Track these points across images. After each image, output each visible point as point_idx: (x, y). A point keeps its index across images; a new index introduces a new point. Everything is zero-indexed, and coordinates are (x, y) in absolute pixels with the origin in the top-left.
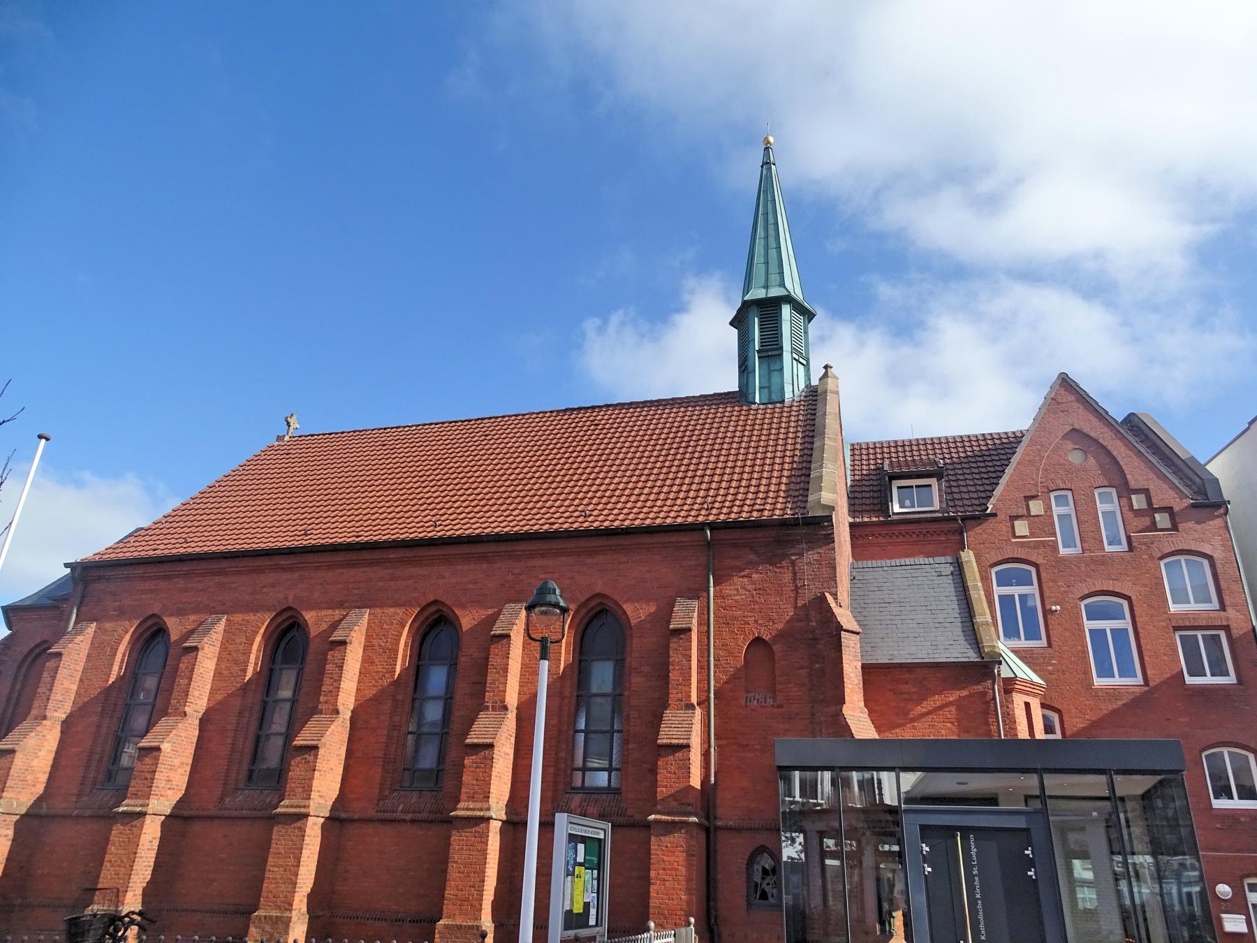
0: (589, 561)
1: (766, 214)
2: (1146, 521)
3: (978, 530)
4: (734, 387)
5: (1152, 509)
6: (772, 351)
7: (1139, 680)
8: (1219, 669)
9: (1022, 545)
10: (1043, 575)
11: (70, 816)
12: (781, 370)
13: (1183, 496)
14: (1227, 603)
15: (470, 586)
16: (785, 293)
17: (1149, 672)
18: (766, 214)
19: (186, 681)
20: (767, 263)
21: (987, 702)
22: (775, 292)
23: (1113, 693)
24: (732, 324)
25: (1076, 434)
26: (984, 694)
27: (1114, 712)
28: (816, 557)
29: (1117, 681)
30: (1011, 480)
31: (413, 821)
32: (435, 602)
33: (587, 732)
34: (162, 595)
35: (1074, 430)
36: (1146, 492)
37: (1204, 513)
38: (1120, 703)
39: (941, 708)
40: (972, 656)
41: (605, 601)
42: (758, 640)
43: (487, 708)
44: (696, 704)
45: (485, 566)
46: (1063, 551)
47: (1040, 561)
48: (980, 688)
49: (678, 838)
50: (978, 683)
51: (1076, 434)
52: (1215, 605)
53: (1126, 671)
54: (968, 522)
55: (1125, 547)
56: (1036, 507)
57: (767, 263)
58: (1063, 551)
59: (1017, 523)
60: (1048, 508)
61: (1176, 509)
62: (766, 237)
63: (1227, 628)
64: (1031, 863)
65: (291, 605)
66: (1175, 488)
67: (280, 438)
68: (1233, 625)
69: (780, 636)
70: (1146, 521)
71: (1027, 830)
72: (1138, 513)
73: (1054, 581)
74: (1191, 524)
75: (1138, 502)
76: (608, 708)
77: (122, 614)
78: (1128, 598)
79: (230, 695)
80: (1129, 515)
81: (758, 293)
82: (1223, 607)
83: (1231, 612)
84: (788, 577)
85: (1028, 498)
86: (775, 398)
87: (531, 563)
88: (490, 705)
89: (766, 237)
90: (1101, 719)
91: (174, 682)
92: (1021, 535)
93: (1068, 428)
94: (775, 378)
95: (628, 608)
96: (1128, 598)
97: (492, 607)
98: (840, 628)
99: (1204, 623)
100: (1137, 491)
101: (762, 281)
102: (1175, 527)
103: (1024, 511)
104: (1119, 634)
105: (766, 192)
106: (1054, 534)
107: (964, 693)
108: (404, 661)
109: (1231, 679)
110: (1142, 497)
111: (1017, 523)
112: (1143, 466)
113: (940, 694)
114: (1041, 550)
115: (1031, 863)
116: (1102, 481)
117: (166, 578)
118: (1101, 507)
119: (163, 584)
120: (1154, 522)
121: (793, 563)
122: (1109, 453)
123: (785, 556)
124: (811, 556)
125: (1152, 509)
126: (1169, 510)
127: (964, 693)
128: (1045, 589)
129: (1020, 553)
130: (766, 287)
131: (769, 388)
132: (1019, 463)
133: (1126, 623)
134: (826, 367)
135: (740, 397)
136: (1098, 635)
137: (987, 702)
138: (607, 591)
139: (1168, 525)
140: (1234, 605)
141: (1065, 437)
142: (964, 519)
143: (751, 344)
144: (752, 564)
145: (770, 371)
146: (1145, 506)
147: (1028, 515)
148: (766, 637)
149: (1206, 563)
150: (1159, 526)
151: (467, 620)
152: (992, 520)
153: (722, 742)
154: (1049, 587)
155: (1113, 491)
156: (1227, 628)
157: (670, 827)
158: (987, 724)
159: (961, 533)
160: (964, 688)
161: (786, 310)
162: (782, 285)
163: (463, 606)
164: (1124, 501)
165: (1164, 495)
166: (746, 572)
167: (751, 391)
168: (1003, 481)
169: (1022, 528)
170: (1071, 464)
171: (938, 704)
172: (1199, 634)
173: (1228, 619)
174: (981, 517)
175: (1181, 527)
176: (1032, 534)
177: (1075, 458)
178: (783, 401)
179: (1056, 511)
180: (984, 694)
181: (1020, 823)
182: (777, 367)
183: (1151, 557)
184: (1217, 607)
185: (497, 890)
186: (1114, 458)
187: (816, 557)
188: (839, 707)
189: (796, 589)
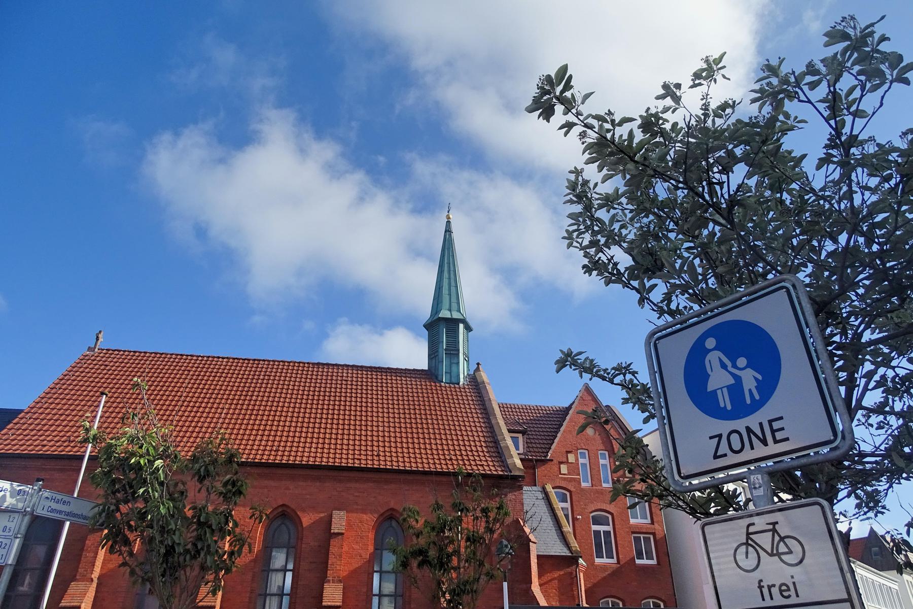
0: (386, 487)
1: (449, 263)
3: (543, 468)
4: (425, 366)
6: (453, 351)
7: (614, 561)
8: (650, 557)
9: (565, 479)
10: (574, 497)
12: (458, 363)
14: (655, 520)
15: (308, 496)
16: (462, 318)
17: (620, 556)
18: (449, 263)
19: (92, 555)
20: (450, 295)
21: (572, 578)
22: (456, 315)
23: (604, 567)
24: (425, 326)
26: (571, 573)
27: (604, 578)
28: (514, 497)
29: (605, 560)
30: (560, 441)
32: (283, 505)
34: (57, 484)
38: (607, 573)
39: (550, 581)
40: (565, 552)
41: (394, 513)
43: (329, 581)
45: (318, 484)
46: (584, 485)
47: (572, 489)
48: (569, 570)
50: (568, 567)
52: (649, 521)
53: (610, 556)
54: (538, 463)
56: (571, 458)
57: (450, 295)
58: (584, 485)
59: (562, 466)
60: (577, 460)
62: (449, 278)
63: (654, 534)
67: (89, 349)
68: (657, 532)
73: (579, 502)
78: (612, 514)
81: (445, 314)
82: (652, 523)
83: (656, 525)
85: (568, 452)
86: (454, 380)
87: (348, 485)
88: (331, 579)
89: (449, 278)
90: (599, 582)
91: (81, 555)
92: (844, 604)
94: (454, 368)
96: (612, 514)
97: (323, 512)
98: (530, 540)
99: (644, 531)
101: (447, 307)
103: (564, 460)
104: (607, 533)
105: (449, 249)
106: (579, 474)
107: (562, 573)
108: (259, 545)
109: (653, 562)
111: (562, 466)
113: (550, 573)
114: (573, 483)
116: (602, 447)
117: (62, 470)
118: (602, 462)
124: (511, 496)
127: (562, 573)
128: (574, 506)
129: (563, 484)
130: (450, 310)
131: (450, 373)
132: (564, 431)
135: (430, 375)
136: (597, 533)
137: (572, 578)
138: (396, 507)
140: (658, 522)
142: (537, 461)
143: (441, 345)
145: (451, 364)
147: (567, 462)
151: (307, 520)
152: (550, 463)
154: (576, 505)
155: (607, 453)
156: (654, 534)
158: (572, 590)
159: (534, 469)
160: (561, 570)
161: (461, 326)
162: (459, 311)
163: (304, 511)
167: (440, 373)
168: (556, 441)
169: (564, 469)
170: (588, 435)
171: (550, 578)
172: (642, 536)
173: (654, 529)
174: (544, 462)
176: (569, 474)
178: (458, 384)
179: (581, 461)
180: (571, 573)
182: (455, 361)
184: (650, 522)
187: (514, 497)
188: (529, 585)
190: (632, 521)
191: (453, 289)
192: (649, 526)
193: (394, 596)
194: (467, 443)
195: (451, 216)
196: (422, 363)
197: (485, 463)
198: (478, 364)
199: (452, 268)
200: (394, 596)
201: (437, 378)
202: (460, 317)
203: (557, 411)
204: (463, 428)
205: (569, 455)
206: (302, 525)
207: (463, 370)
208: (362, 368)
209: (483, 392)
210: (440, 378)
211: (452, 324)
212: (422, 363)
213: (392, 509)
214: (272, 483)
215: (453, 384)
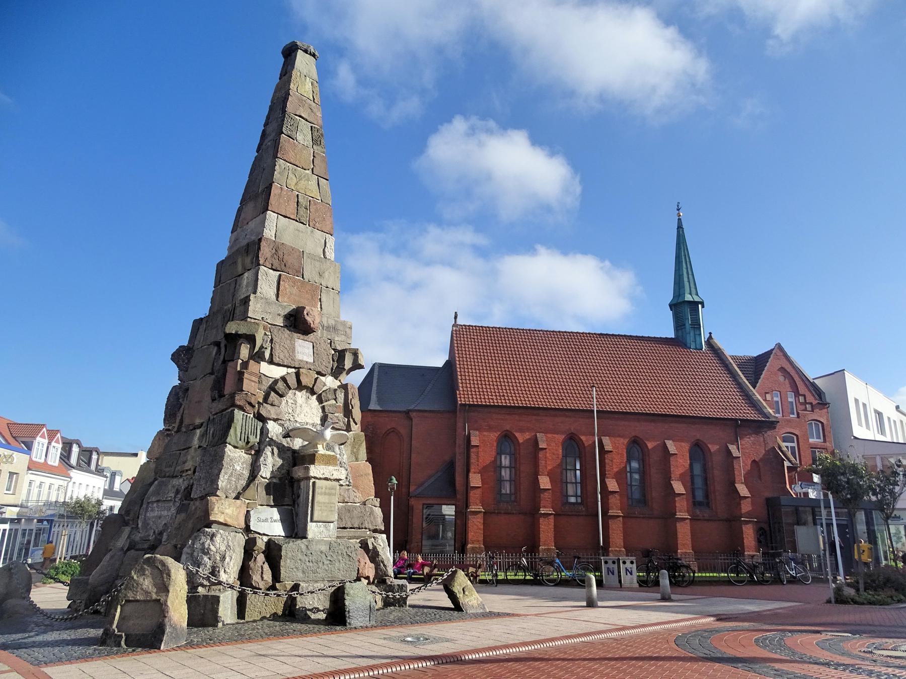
2: (803, 407)
5: (805, 403)
11: (494, 513)
13: (816, 399)
22: (697, 299)
25: (782, 369)
31: (643, 518)
33: (576, 470)
35: (782, 367)
36: (804, 396)
37: (821, 406)
42: (754, 461)
44: (323, 404)
45: (653, 424)
49: (750, 526)
51: (782, 369)
52: (822, 440)
55: (795, 416)
57: (689, 282)
60: (772, 398)
61: (814, 404)
62: (687, 268)
64: (847, 533)
65: (573, 432)
66: (814, 396)
69: (761, 460)
70: (803, 407)
71: (847, 525)
72: (801, 404)
74: (818, 410)
75: (801, 399)
76: (472, 438)
77: (490, 429)
78: (797, 436)
79: (555, 467)
80: (798, 404)
81: (688, 298)
84: (762, 439)
87: (671, 425)
93: (780, 366)
94: (698, 339)
95: (710, 446)
100: (802, 395)
102: (813, 411)
110: (803, 397)
112: (804, 385)
115: (847, 533)
117: (508, 414)
119: (507, 417)
120: (806, 408)
121: (763, 435)
122: (793, 378)
123: (761, 432)
124: (769, 433)
125: (805, 403)
126: (811, 404)
130: (691, 294)
133: (795, 445)
134: (710, 333)
135: (678, 342)
138: (701, 439)
139: (810, 409)
141: (778, 370)
143: (687, 321)
144: (750, 434)
146: (803, 401)
148: (757, 460)
149: (820, 425)
150: (808, 409)
153: (839, 510)
157: (747, 522)
162: (697, 294)
163: (648, 440)
164: (797, 399)
165: (810, 398)
166: (748, 437)
175: (815, 411)
177: (781, 378)
181: (845, 523)
183: (805, 421)
185: (307, 517)
186: (795, 381)
189: (765, 444)
190: (811, 440)
191: (690, 276)
192: (823, 444)
193: (510, 467)
194: (533, 338)
195: (681, 214)
196: (669, 332)
197: (476, 337)
198: (710, 333)
199: (688, 260)
200: (510, 467)
201: (686, 345)
202: (700, 300)
203: (749, 360)
204: (584, 341)
205: (767, 395)
206: (648, 448)
207: (704, 338)
208: (631, 337)
209: (723, 357)
210: (688, 345)
211: (694, 305)
212: (669, 332)
213: (698, 440)
214: (626, 423)
215: (699, 350)
